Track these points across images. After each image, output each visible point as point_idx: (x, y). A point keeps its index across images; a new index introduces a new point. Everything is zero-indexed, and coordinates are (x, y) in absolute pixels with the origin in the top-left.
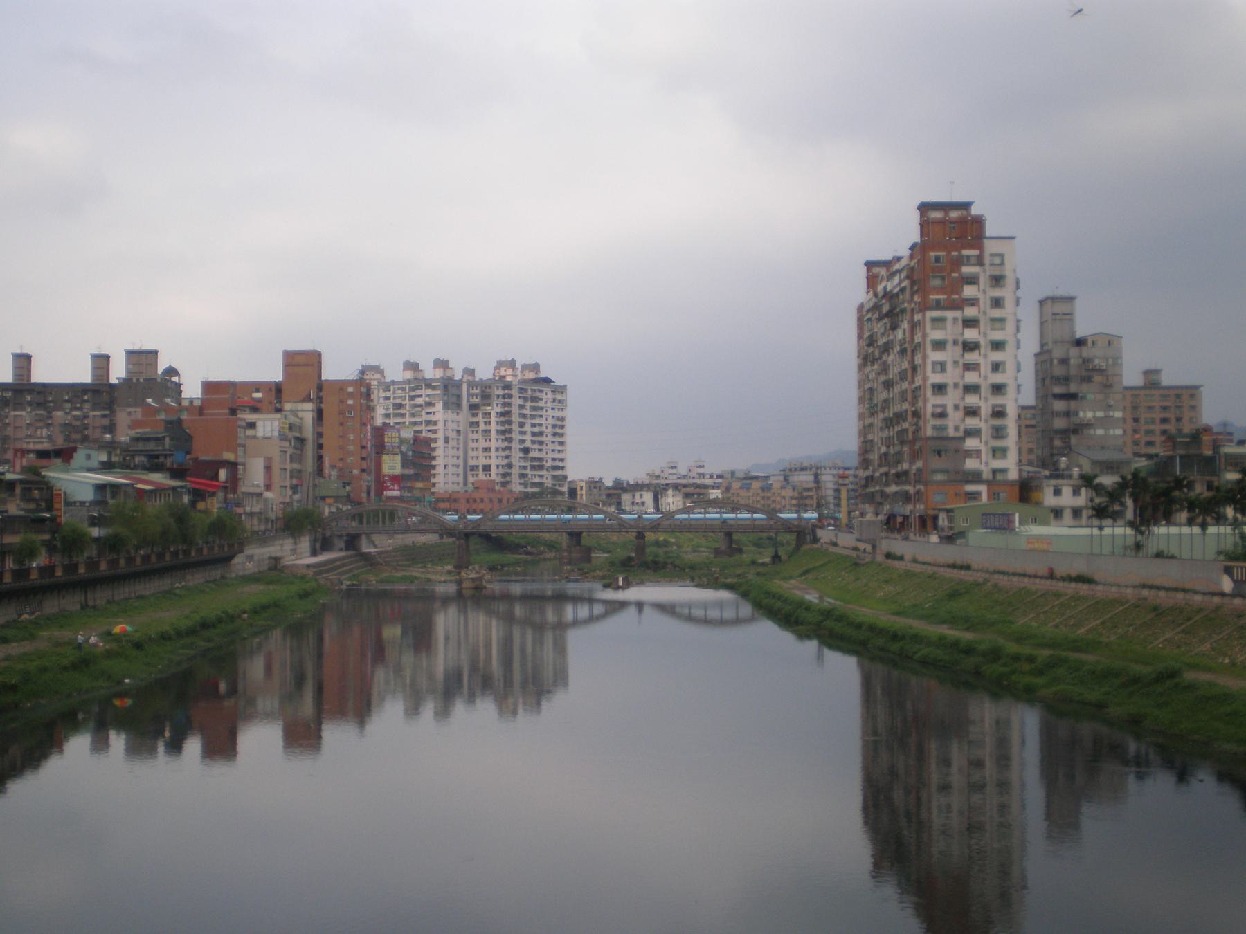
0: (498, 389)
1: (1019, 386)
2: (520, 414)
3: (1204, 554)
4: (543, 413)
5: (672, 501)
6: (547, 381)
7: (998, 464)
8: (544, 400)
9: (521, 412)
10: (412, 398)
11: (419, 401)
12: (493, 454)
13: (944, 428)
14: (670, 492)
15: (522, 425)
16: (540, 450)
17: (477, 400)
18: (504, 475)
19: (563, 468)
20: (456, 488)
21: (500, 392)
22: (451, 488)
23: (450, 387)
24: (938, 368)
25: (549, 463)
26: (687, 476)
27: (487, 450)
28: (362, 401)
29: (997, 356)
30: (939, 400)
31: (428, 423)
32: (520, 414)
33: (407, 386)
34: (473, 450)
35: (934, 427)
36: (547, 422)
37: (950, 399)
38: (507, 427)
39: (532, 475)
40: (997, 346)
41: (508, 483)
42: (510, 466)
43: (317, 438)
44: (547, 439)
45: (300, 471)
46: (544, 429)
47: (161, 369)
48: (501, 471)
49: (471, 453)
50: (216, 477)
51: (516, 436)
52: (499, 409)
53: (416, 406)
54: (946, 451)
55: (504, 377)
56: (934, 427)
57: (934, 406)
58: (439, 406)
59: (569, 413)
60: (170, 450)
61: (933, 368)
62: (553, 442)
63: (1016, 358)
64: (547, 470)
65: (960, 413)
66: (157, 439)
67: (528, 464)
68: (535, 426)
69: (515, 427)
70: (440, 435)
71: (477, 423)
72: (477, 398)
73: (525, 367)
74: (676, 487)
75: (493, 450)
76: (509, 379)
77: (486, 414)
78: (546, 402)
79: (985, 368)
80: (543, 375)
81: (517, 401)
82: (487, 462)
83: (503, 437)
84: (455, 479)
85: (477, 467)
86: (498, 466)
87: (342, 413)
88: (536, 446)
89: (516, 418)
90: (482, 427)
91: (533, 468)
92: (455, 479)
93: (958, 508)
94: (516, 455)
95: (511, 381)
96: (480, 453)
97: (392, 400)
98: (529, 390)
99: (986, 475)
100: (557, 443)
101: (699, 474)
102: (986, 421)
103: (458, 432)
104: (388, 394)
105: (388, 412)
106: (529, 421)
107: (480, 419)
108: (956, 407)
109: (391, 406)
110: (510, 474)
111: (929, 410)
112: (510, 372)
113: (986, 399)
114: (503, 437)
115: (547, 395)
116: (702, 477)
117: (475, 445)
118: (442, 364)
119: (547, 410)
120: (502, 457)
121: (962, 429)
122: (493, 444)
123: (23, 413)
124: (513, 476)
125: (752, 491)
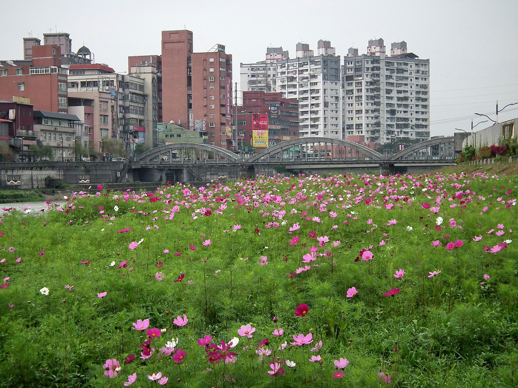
0: (368, 63)
2: (387, 83)
4: (408, 82)
6: (412, 56)
8: (409, 72)
9: (388, 81)
10: (301, 72)
11: (306, 74)
15: (389, 92)
16: (405, 112)
18: (373, 132)
19: (426, 126)
21: (370, 65)
25: (414, 122)
31: (312, 91)
32: (387, 83)
33: (297, 63)
38: (375, 93)
41: (377, 138)
42: (378, 124)
43: (188, 100)
45: (141, 121)
46: (408, 94)
47: (75, 50)
48: (370, 128)
50: (7, 116)
51: (384, 100)
52: (369, 79)
53: (303, 78)
58: (320, 78)
62: (417, 112)
64: (412, 128)
67: (394, 123)
69: (383, 93)
71: (352, 91)
73: (394, 45)
75: (364, 111)
77: (358, 83)
78: (411, 73)
80: (409, 51)
81: (384, 72)
82: (359, 122)
83: (373, 102)
85: (352, 125)
86: (368, 125)
87: (205, 79)
88: (402, 109)
89: (383, 87)
90: (355, 94)
94: (384, 116)
95: (379, 57)
96: (354, 115)
97: (286, 75)
100: (420, 106)
104: (284, 69)
105: (284, 84)
106: (395, 89)
107: (354, 87)
109: (286, 80)
110: (378, 131)
114: (373, 102)
115: (412, 67)
117: (350, 108)
119: (411, 80)
120: (372, 117)
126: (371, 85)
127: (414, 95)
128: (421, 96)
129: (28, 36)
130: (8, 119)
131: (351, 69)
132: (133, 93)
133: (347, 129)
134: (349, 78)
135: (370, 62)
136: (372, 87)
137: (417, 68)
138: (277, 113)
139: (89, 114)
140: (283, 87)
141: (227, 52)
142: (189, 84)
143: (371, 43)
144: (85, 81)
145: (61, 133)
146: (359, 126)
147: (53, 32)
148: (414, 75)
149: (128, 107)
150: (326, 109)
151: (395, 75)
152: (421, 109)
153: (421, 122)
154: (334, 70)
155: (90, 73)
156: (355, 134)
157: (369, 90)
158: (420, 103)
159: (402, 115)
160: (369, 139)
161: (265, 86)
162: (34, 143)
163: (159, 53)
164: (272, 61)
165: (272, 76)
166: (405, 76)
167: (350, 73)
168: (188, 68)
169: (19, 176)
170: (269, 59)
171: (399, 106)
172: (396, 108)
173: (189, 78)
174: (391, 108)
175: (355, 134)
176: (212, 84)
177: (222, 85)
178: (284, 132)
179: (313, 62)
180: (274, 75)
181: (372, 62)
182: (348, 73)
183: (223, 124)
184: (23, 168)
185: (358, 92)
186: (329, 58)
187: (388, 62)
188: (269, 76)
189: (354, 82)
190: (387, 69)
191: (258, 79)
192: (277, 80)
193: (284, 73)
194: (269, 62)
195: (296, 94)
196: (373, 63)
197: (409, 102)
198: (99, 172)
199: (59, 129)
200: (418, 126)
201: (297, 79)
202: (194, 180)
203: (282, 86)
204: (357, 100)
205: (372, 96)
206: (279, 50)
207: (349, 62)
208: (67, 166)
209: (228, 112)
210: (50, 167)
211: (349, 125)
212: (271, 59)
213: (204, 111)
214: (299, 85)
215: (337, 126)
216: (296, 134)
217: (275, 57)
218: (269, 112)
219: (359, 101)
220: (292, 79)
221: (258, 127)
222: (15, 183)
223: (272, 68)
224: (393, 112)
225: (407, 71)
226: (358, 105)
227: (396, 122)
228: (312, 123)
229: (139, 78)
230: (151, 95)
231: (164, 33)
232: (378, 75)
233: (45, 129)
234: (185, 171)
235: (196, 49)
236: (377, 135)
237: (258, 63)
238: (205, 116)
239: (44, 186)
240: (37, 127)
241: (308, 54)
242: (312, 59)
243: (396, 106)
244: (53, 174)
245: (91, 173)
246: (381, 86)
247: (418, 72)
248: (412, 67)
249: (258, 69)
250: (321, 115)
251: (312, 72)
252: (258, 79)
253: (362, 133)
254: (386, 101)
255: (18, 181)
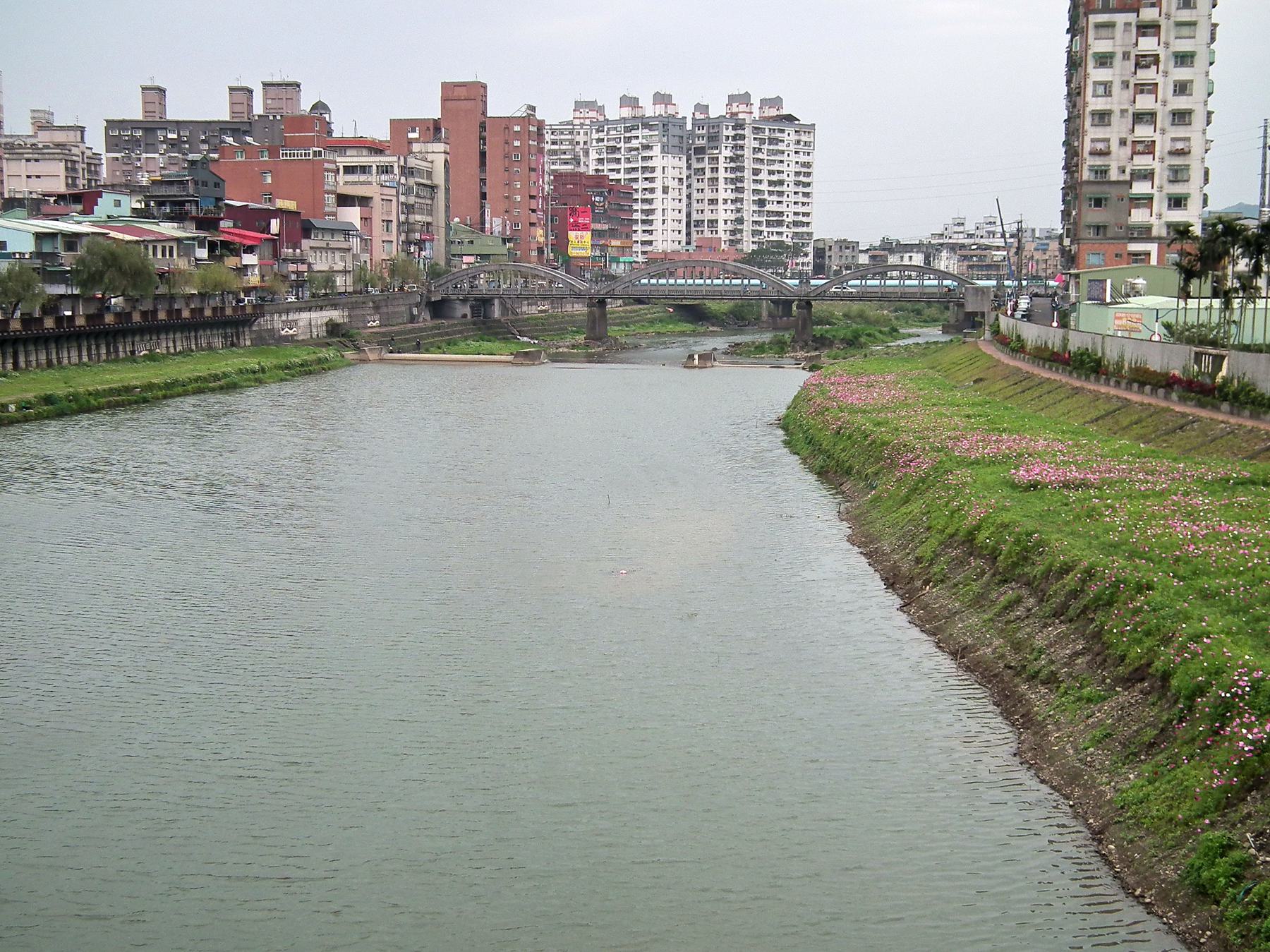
0: (727, 129)
1: (1209, 114)
3: (1264, 339)
4: (785, 157)
5: (946, 262)
6: (790, 119)
7: (1177, 216)
8: (786, 142)
9: (756, 156)
10: (628, 140)
11: (635, 144)
12: (721, 206)
13: (1104, 171)
14: (944, 254)
15: (756, 172)
16: (779, 202)
17: (703, 142)
18: (733, 232)
19: (808, 224)
20: (676, 246)
21: (731, 133)
22: (670, 247)
23: (670, 126)
24: (1101, 90)
26: (943, 235)
27: (713, 202)
28: (531, 142)
29: (1182, 74)
30: (1100, 133)
31: (645, 169)
33: (623, 126)
34: (698, 202)
35: (1091, 169)
36: (789, 169)
37: (1117, 129)
38: (739, 174)
39: (768, 232)
40: (1184, 59)
41: (739, 241)
42: (740, 221)
43: (481, 187)
44: (789, 189)
45: (429, 224)
46: (784, 176)
47: (306, 106)
48: (730, 226)
49: (695, 205)
50: (267, 229)
51: (748, 185)
52: (728, 153)
53: (631, 149)
54: (1106, 199)
55: (736, 114)
56: (1091, 169)
57: (1093, 141)
58: (657, 150)
59: (817, 158)
60: (193, 196)
61: (1094, 91)
62: (795, 203)
63: (1207, 75)
64: (788, 226)
65: (1128, 150)
66: (181, 182)
67: (763, 219)
68: (774, 174)
69: (747, 174)
70: (658, 185)
71: (703, 169)
72: (703, 140)
73: (764, 102)
74: (953, 248)
75: (720, 201)
76: (741, 116)
77: (713, 159)
78: (788, 145)
79: (1165, 89)
80: (785, 112)
81: (750, 143)
82: (713, 217)
83: (733, 187)
84: (676, 236)
87: (507, 156)
88: (775, 198)
89: (748, 164)
90: (708, 174)
91: (769, 224)
92: (676, 236)
93: (1083, 273)
94: (749, 208)
95: (744, 119)
96: (706, 206)
97: (605, 143)
98: (767, 131)
99: (1159, 230)
100: (801, 194)
101: (989, 232)
102: (1162, 160)
103: (680, 180)
104: (601, 135)
105: (601, 157)
106: (765, 168)
107: (706, 165)
108: (1123, 142)
109: (604, 150)
110: (741, 231)
111: (1088, 146)
112: (743, 108)
113: (1163, 131)
114: (733, 187)
115: (789, 136)
116: (991, 236)
117: (700, 196)
118: (662, 99)
119: (788, 155)
121: (1128, 171)
122: (722, 195)
123: (156, 156)
124: (745, 233)
125: (1048, 253)
126: (731, 162)
127: (792, 178)
128: (802, 178)
129: (235, 84)
130: (269, 232)
131: (703, 137)
132: (419, 184)
133: (695, 226)
134: (700, 150)
135: (730, 128)
136: (733, 165)
137: (797, 138)
138: (604, 206)
139: (366, 219)
140: (600, 161)
141: (539, 116)
142: (483, 163)
143: (732, 99)
144: (357, 164)
145: (334, 250)
146: (713, 223)
147: (277, 79)
148: (792, 147)
149: (413, 205)
150: (665, 196)
151: (766, 147)
152: (801, 199)
153: (800, 218)
154: (677, 138)
155: (354, 152)
156: (707, 234)
157: (729, 170)
158: (801, 189)
159: (775, 208)
160: (727, 243)
161: (572, 159)
162: (303, 268)
163: (437, 115)
164: (582, 121)
165: (582, 144)
166: (780, 148)
167: (701, 143)
168: (480, 139)
169: (295, 321)
170: (577, 118)
171: (771, 193)
172: (766, 196)
173: (483, 155)
174: (759, 197)
175: (707, 234)
176: (516, 164)
177: (533, 166)
178: (613, 233)
179: (646, 126)
180: (585, 143)
181: (734, 128)
182: (697, 142)
183: (532, 224)
184: (301, 310)
185: (712, 172)
186: (670, 120)
187: (756, 128)
188: (578, 143)
189: (707, 157)
190: (755, 139)
191: (562, 147)
192: (590, 151)
193: (602, 140)
194: (577, 122)
195: (619, 173)
196: (736, 130)
197: (784, 188)
198: (391, 309)
199: (332, 245)
200: (796, 224)
201: (622, 150)
202: (508, 315)
203: (599, 159)
204: (711, 183)
205: (732, 179)
206: (591, 105)
207: (699, 127)
208: (352, 303)
209: (540, 206)
210: (332, 306)
211: (698, 221)
212: (580, 118)
213: (503, 206)
214: (625, 158)
215: (680, 221)
216: (628, 236)
217: (587, 115)
218: (593, 204)
219: (713, 185)
220: (614, 150)
221: (577, 227)
222: (291, 332)
223: (582, 131)
224: (762, 203)
225: (783, 141)
226: (712, 191)
227: (765, 218)
228: (644, 218)
229: (426, 160)
230: (443, 188)
231: (445, 86)
232: (742, 148)
233: (318, 245)
234: (496, 302)
235: (492, 112)
236: (739, 236)
237: (561, 124)
238: (507, 212)
239: (325, 334)
240: (306, 244)
241: (638, 113)
242: (644, 120)
243: (766, 192)
244: (335, 315)
245: (381, 311)
246: (746, 164)
247: (798, 142)
248: (789, 136)
249: (562, 133)
250: (657, 205)
251: (644, 141)
252: (562, 147)
253: (716, 233)
254: (753, 187)
255: (295, 329)
